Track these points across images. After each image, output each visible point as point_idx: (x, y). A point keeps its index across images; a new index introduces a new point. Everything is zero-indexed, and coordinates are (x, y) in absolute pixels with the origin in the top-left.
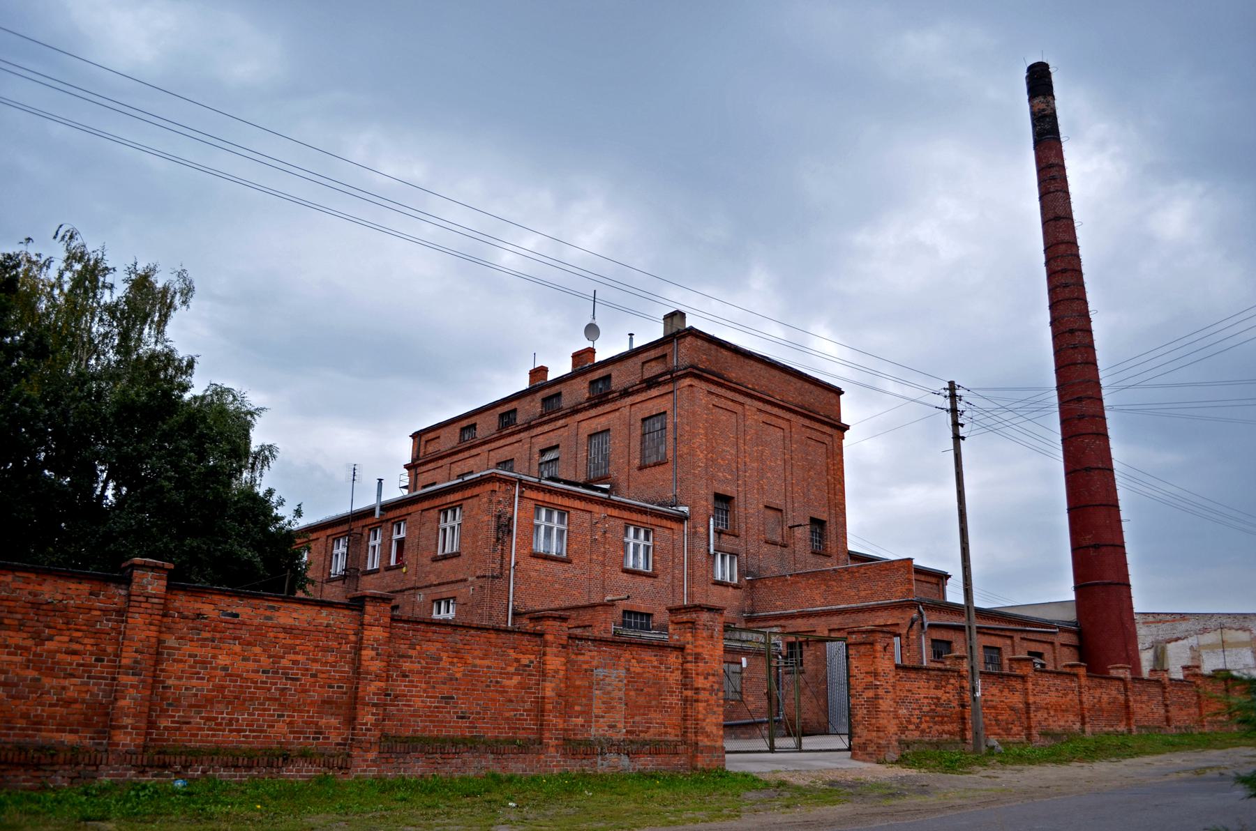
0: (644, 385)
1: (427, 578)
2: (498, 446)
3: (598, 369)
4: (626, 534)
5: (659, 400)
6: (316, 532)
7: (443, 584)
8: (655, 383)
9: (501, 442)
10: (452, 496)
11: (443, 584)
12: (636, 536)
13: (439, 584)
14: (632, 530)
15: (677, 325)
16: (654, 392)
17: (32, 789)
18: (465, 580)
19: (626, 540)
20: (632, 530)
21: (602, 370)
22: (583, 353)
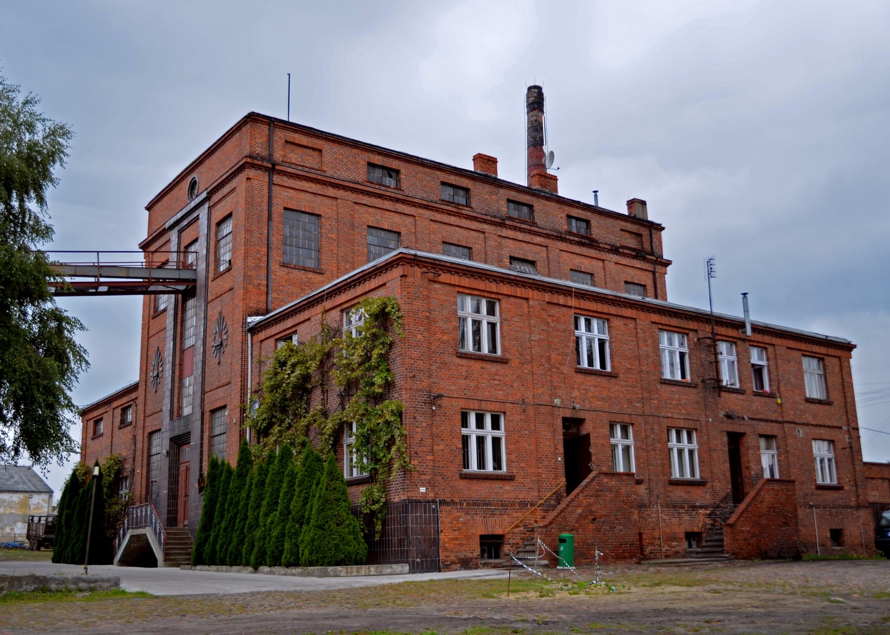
0: (634, 253)
1: (804, 417)
2: (406, 212)
3: (577, 207)
4: (612, 434)
5: (639, 272)
6: (780, 337)
7: (820, 426)
8: (641, 257)
9: (453, 220)
10: (817, 347)
11: (820, 426)
12: (679, 440)
13: (817, 425)
14: (472, 419)
15: (637, 209)
16: (637, 263)
17: (284, 528)
18: (840, 428)
19: (613, 441)
20: (472, 419)
21: (580, 211)
22: (551, 178)
